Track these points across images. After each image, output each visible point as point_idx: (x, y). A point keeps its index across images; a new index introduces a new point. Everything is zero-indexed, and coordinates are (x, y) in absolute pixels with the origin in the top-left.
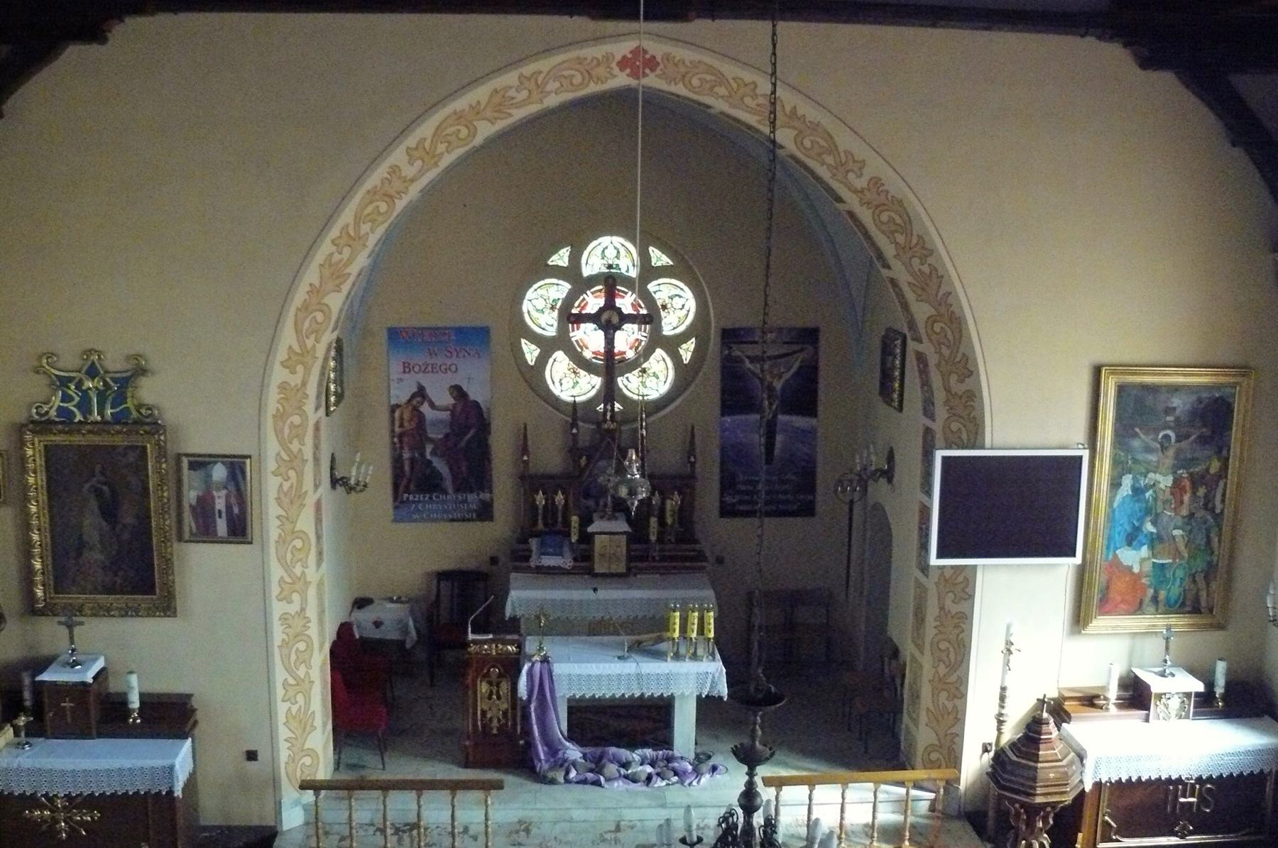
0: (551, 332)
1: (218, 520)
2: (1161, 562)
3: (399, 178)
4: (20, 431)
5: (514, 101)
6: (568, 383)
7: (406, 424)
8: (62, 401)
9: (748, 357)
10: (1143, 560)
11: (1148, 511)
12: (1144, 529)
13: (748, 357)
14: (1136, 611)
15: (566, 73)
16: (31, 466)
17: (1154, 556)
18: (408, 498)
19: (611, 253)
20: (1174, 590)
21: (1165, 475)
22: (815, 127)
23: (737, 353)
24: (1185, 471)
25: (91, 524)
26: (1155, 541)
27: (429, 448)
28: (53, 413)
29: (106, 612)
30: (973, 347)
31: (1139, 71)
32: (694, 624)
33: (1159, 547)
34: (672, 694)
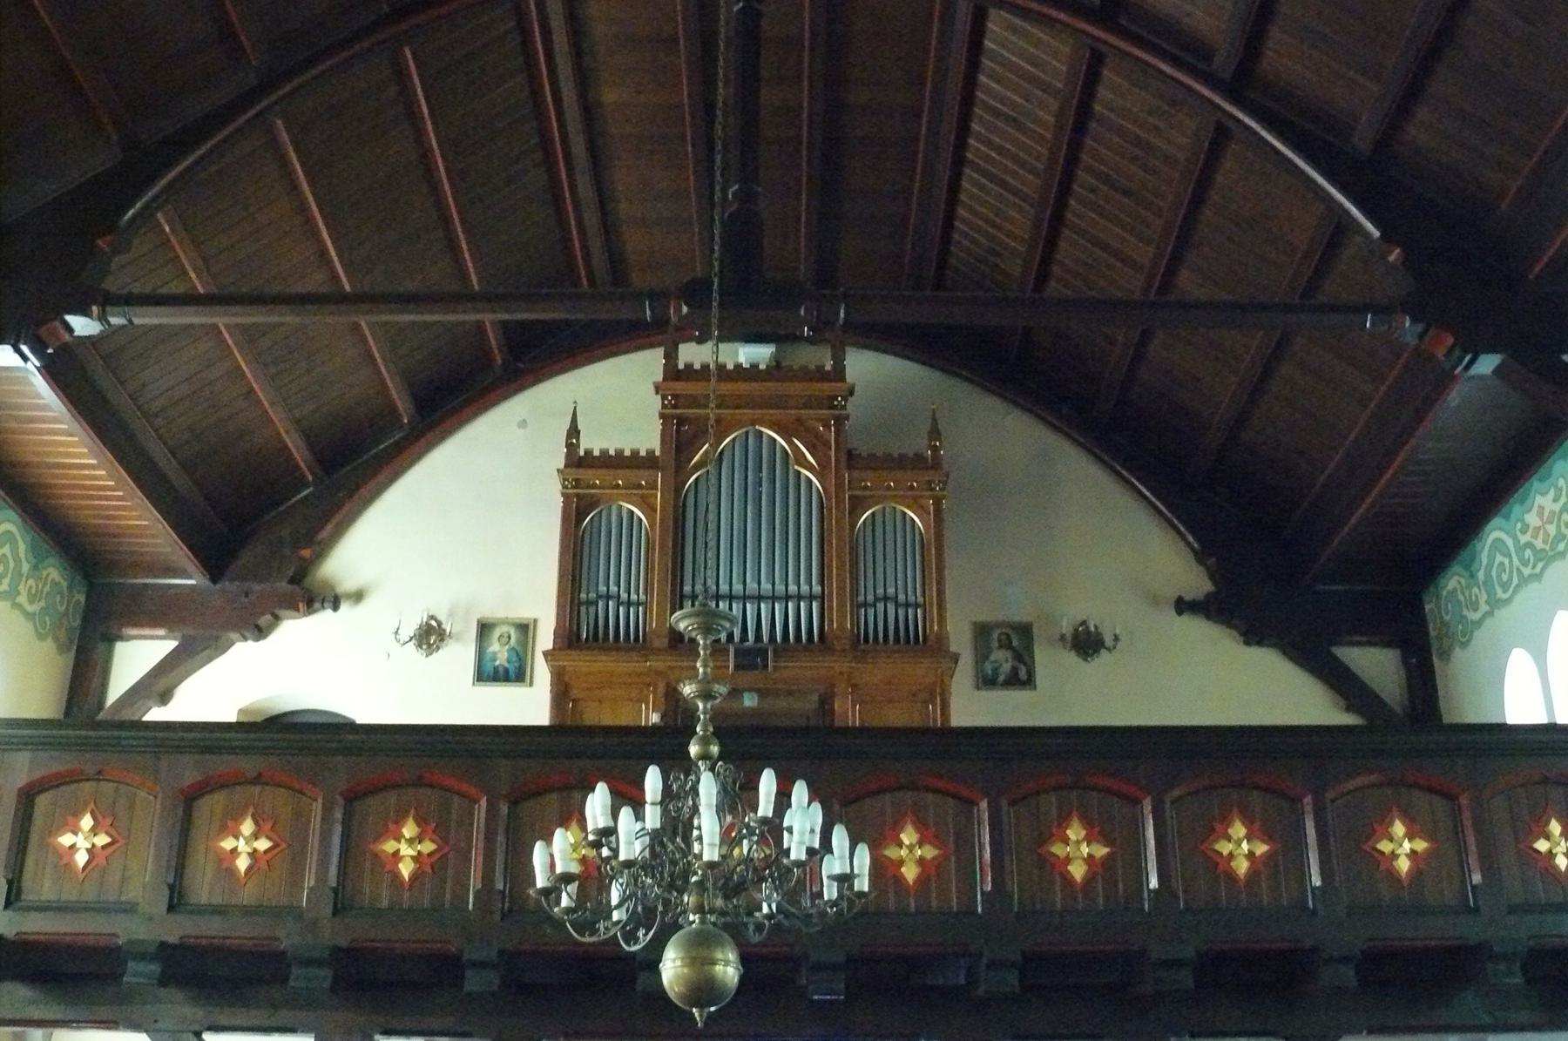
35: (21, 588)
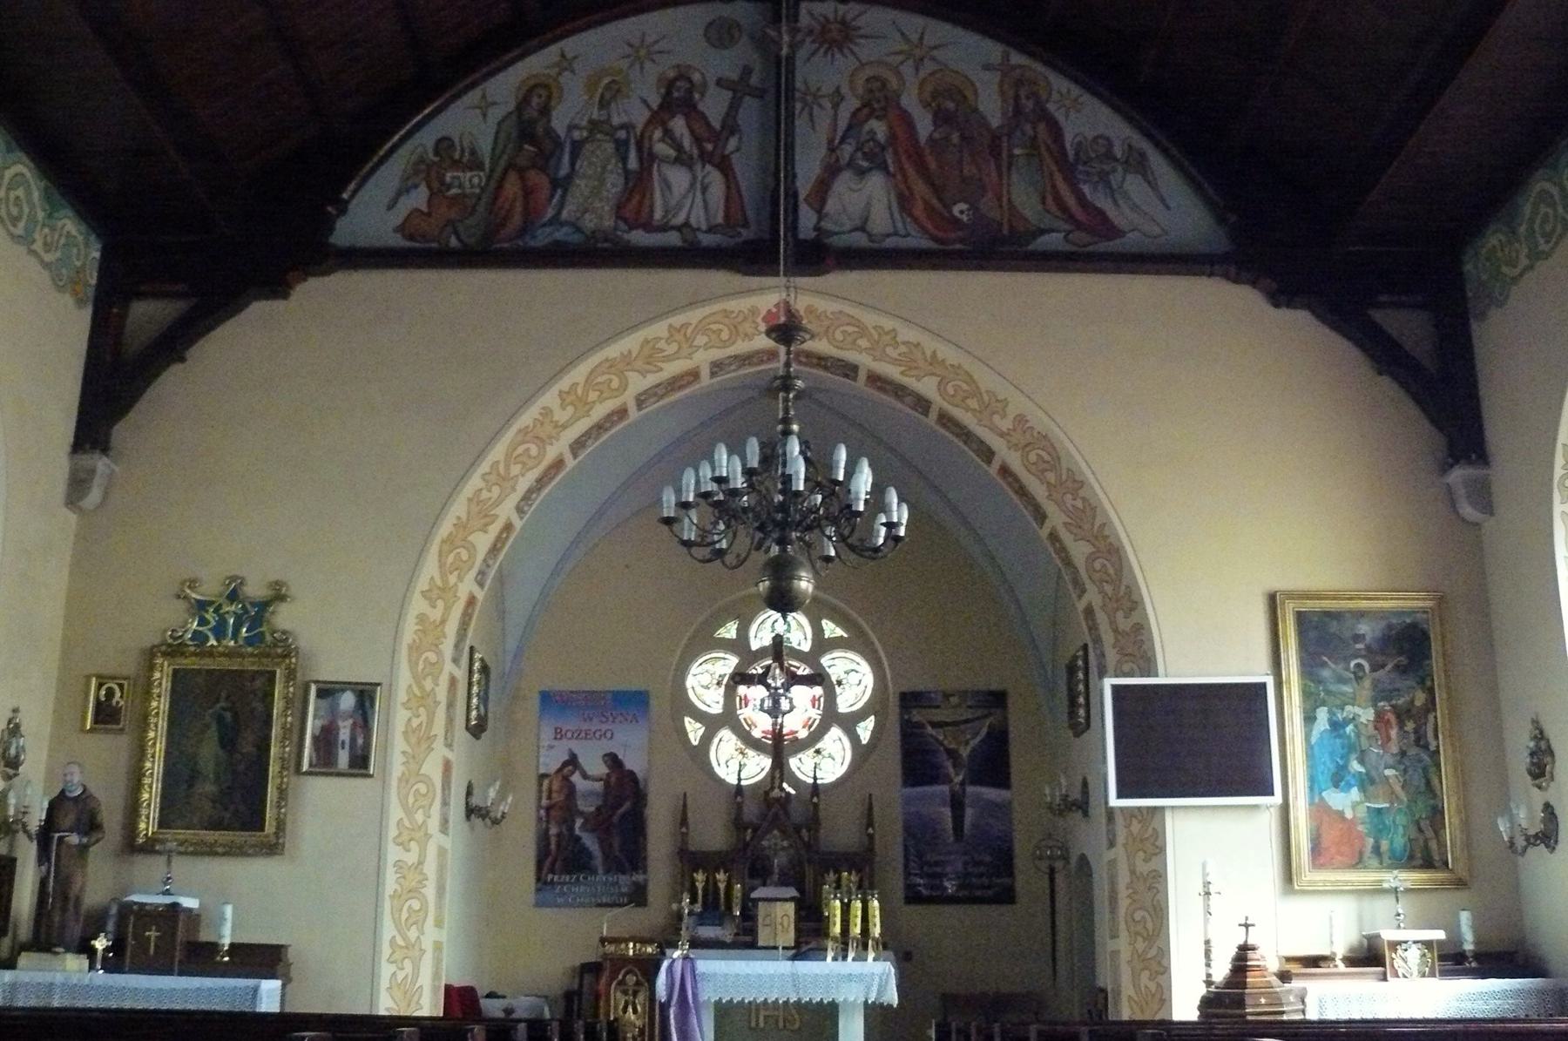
0: (717, 709)
2: (1377, 806)
3: (552, 422)
7: (554, 795)
12: (1350, 768)
14: (1357, 864)
15: (714, 327)
16: (156, 691)
17: (1368, 799)
18: (552, 880)
20: (1398, 840)
22: (957, 368)
24: (1387, 704)
25: (208, 752)
26: (1367, 783)
27: (579, 822)
30: (1135, 577)
31: (1271, 310)
32: (856, 916)
34: (833, 1000)
35: (37, 236)
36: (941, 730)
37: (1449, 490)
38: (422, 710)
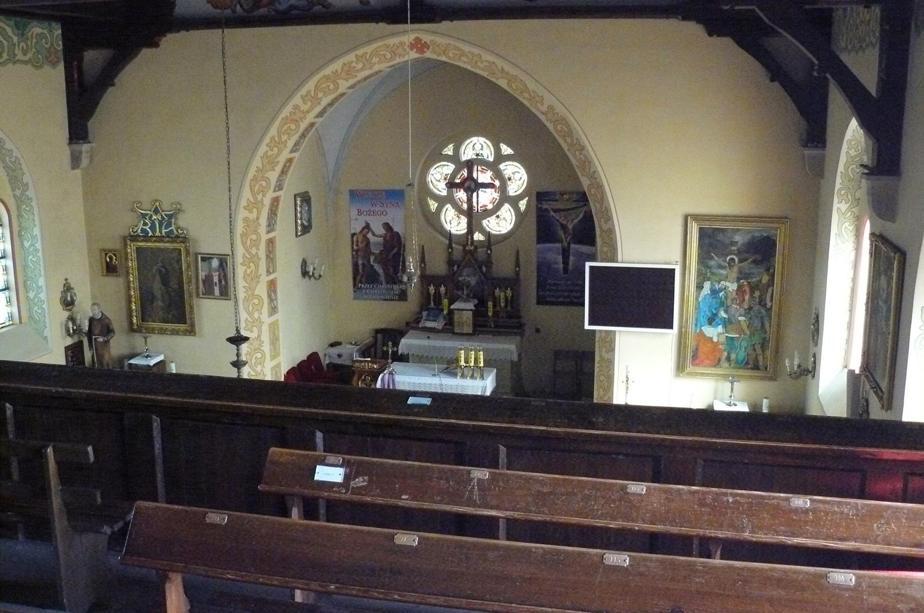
1: (215, 287)
2: (731, 336)
4: (125, 240)
5: (356, 69)
6: (454, 223)
7: (360, 244)
8: (143, 225)
9: (553, 209)
10: (719, 335)
11: (722, 304)
12: (719, 315)
13: (553, 209)
14: (716, 365)
17: (727, 332)
18: (361, 287)
19: (478, 147)
21: (733, 283)
22: (515, 77)
23: (545, 206)
26: (727, 323)
27: (372, 258)
28: (139, 231)
29: (162, 332)
33: (729, 327)
36: (558, 214)
37: (804, 157)
38: (251, 264)
